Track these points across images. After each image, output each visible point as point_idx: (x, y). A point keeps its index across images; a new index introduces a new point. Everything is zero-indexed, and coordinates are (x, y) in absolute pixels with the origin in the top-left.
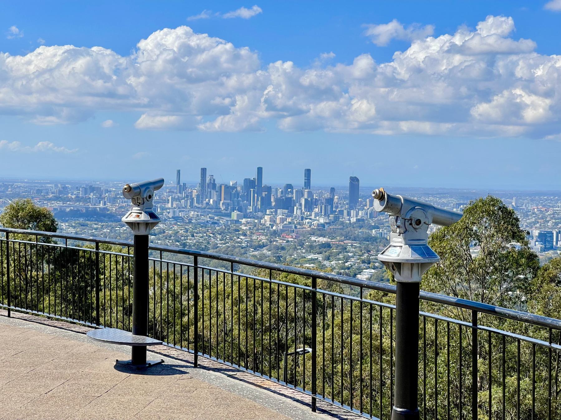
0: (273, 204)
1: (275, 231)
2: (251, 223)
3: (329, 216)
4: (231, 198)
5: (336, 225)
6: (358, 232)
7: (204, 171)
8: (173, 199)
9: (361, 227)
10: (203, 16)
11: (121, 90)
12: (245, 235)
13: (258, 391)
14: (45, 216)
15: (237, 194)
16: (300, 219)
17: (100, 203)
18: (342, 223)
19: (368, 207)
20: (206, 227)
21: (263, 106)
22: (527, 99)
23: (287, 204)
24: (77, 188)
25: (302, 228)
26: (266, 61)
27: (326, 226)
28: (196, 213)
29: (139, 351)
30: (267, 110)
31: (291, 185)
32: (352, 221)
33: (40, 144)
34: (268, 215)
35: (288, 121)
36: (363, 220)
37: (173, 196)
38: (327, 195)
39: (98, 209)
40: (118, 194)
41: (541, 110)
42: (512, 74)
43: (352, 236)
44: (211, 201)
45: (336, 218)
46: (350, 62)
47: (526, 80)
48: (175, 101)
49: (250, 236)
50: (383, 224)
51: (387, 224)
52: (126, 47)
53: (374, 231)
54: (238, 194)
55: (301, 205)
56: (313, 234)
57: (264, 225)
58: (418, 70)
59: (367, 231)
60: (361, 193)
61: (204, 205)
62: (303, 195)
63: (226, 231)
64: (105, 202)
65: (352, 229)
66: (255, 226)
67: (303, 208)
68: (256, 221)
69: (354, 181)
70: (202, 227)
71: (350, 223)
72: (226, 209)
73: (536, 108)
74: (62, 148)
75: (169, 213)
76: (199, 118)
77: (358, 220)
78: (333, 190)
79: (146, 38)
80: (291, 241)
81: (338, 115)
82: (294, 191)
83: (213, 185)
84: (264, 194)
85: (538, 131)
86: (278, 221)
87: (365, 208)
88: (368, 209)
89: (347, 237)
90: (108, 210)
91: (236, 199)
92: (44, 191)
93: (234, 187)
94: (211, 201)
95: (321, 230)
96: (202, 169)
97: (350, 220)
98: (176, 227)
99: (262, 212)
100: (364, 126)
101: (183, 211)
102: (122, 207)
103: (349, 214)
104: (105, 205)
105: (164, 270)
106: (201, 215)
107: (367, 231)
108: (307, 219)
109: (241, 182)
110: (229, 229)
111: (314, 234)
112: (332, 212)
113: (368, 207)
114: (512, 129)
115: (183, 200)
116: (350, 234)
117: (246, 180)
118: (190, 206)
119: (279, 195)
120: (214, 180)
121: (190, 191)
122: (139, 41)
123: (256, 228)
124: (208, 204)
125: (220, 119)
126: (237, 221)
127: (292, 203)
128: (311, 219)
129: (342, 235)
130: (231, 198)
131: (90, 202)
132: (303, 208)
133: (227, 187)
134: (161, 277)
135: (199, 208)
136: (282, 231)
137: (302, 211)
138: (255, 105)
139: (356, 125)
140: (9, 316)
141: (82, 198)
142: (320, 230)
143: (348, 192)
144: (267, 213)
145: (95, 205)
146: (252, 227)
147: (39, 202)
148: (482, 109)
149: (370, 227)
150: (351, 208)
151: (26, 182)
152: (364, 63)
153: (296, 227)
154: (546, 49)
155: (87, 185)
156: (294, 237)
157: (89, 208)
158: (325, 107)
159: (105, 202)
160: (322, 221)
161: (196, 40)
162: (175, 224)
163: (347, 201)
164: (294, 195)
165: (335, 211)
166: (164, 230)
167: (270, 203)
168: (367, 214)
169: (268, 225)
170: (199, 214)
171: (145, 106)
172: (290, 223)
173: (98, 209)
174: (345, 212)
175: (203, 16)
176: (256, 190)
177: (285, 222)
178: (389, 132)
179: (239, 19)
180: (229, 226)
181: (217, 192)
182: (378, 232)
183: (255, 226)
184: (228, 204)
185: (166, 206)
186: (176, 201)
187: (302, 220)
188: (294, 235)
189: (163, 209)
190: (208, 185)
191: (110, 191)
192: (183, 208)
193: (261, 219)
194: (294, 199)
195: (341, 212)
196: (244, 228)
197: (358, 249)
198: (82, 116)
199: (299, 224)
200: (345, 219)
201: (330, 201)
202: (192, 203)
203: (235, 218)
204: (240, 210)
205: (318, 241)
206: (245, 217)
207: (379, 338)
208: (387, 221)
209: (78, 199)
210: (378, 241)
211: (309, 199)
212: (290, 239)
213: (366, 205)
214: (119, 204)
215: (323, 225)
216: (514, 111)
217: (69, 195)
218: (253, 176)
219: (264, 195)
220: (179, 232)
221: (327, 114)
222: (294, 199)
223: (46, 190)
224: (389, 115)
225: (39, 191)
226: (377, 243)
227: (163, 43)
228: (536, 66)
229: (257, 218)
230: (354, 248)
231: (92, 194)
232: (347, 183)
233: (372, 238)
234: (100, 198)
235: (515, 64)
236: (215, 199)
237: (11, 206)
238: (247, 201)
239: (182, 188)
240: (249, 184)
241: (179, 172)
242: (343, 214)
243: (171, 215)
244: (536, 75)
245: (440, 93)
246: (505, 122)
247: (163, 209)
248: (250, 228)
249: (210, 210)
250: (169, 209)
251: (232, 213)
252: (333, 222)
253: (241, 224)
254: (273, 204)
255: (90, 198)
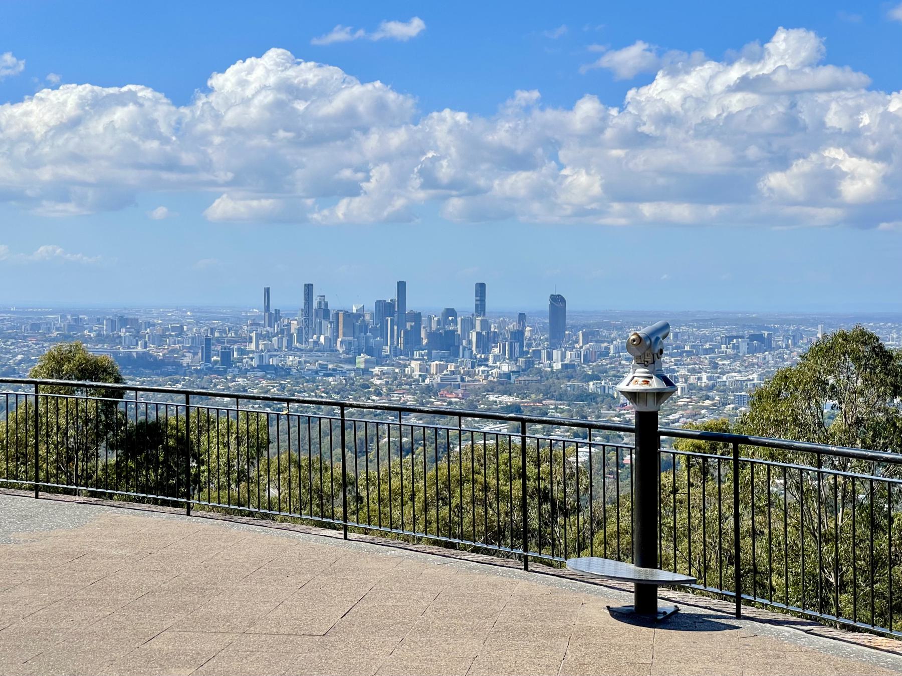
0: (425, 342)
1: (428, 386)
2: (387, 373)
3: (516, 360)
4: (354, 332)
5: (528, 375)
6: (566, 385)
7: (309, 288)
8: (259, 336)
9: (570, 378)
10: (339, 35)
11: (188, 158)
12: (379, 394)
13: (890, 657)
14: (105, 370)
15: (365, 327)
16: (470, 365)
17: (137, 344)
18: (539, 371)
19: (581, 344)
20: (314, 382)
21: (417, 182)
22: (848, 163)
23: (446, 343)
24: (98, 319)
25: (473, 381)
26: (429, 105)
27: (513, 378)
28: (297, 359)
29: (646, 592)
30: (423, 187)
31: (453, 310)
32: (555, 368)
33: (42, 248)
34: (417, 360)
35: (456, 204)
36: (573, 366)
37: (259, 332)
38: (513, 326)
39: (134, 354)
40: (168, 329)
41: (869, 183)
42: (822, 124)
43: (557, 393)
44: (322, 338)
45: (529, 364)
46: (570, 106)
47: (846, 134)
48: (266, 175)
49: (388, 395)
50: (606, 372)
51: (612, 373)
52: (185, 87)
53: (591, 383)
54: (366, 326)
55: (470, 342)
56: (491, 390)
57: (410, 376)
58: (667, 119)
59: (580, 384)
60: (569, 321)
61: (311, 345)
62: (473, 327)
63: (348, 387)
64: (146, 343)
65: (556, 381)
66: (396, 379)
67: (474, 348)
68: (397, 370)
69: (557, 301)
70: (308, 381)
71: (552, 371)
72: (347, 352)
73: (860, 178)
74: (79, 256)
75: (252, 359)
76: (309, 202)
77: (565, 366)
78: (522, 317)
79: (223, 71)
80: (456, 402)
81: (542, 193)
82: (459, 319)
83: (325, 312)
84: (408, 326)
85: (865, 216)
86: (433, 370)
87: (577, 346)
88: (581, 347)
89: (548, 394)
90: (151, 356)
91: (362, 334)
92: (43, 326)
93: (360, 315)
94: (322, 338)
95: (504, 384)
96: (312, 285)
97: (551, 367)
98: (264, 383)
99: (407, 355)
100: (582, 212)
101: (276, 356)
102: (174, 351)
103: (550, 357)
104: (145, 348)
105: (304, 456)
106: (306, 362)
107: (580, 384)
108: (481, 366)
109: (371, 306)
110: (352, 384)
111: (492, 391)
112: (522, 353)
113: (581, 344)
114: (827, 213)
115: (276, 338)
116: (552, 389)
117: (378, 302)
118: (287, 347)
119: (434, 326)
120: (326, 304)
121: (286, 322)
122: (209, 76)
123: (397, 382)
124: (316, 343)
125: (344, 202)
126: (365, 371)
127: (456, 340)
128: (487, 366)
129: (538, 391)
130: (354, 332)
131: (120, 343)
132: (474, 348)
133: (348, 315)
134: (300, 467)
135: (302, 350)
136: (440, 386)
137: (472, 352)
138: (401, 181)
139: (569, 211)
140: (346, 538)
141: (108, 336)
142: (503, 384)
143: (548, 321)
144: (415, 357)
145: (129, 348)
146: (390, 380)
147: (36, 344)
148: (776, 180)
149: (584, 378)
150: (553, 346)
151: (14, 312)
152: (587, 108)
153: (463, 380)
154: (886, 83)
155: (116, 315)
156: (460, 395)
157: (120, 353)
158: (519, 182)
159: (146, 343)
160: (505, 368)
161: (309, 73)
162: (263, 377)
163: (547, 336)
164: (459, 326)
165: (528, 352)
166: (244, 387)
167: (420, 339)
168: (579, 356)
169: (417, 377)
170: (302, 360)
171: (227, 184)
172: (453, 373)
173: (134, 354)
174: (544, 354)
175: (339, 35)
176: (396, 319)
177: (445, 372)
178: (623, 221)
179: (392, 43)
180: (352, 379)
181: (331, 323)
182: (599, 385)
183: (396, 379)
184: (350, 343)
185: (248, 348)
186: (264, 340)
187: (473, 367)
188: (460, 392)
189: (242, 352)
190: (315, 312)
191: (154, 325)
192: (275, 350)
193: (405, 366)
194: (459, 332)
195: (537, 353)
196: (378, 382)
197: (565, 414)
198: (116, 200)
199: (468, 374)
200: (543, 364)
201: (518, 335)
202: (290, 342)
203: (362, 367)
204: (369, 352)
205: (500, 402)
206: (378, 364)
207: (672, 561)
208: (612, 368)
209: (100, 338)
210: (599, 399)
211: (484, 333)
212: (454, 400)
213: (577, 342)
214: (169, 346)
215: (508, 376)
216: (827, 184)
217: (86, 332)
218: (390, 295)
219: (408, 327)
220: (269, 390)
221: (522, 192)
222: (459, 332)
223: (47, 324)
224: (624, 191)
225: (35, 327)
226: (597, 403)
227: (251, 82)
228: (859, 110)
229: (398, 365)
230: (561, 413)
231: (123, 330)
232: (545, 305)
233: (589, 395)
234: (137, 336)
235: (826, 108)
236: (328, 334)
237: (50, 354)
238: (382, 337)
239: (274, 317)
240: (385, 309)
241: (267, 291)
242: (540, 357)
243: (255, 363)
244: (861, 125)
245: (711, 155)
246: (812, 201)
247: (242, 352)
248: (387, 382)
249: (319, 354)
250: (252, 352)
251: (358, 357)
252: (523, 371)
253: (372, 375)
254: (425, 342)
255: (120, 337)
